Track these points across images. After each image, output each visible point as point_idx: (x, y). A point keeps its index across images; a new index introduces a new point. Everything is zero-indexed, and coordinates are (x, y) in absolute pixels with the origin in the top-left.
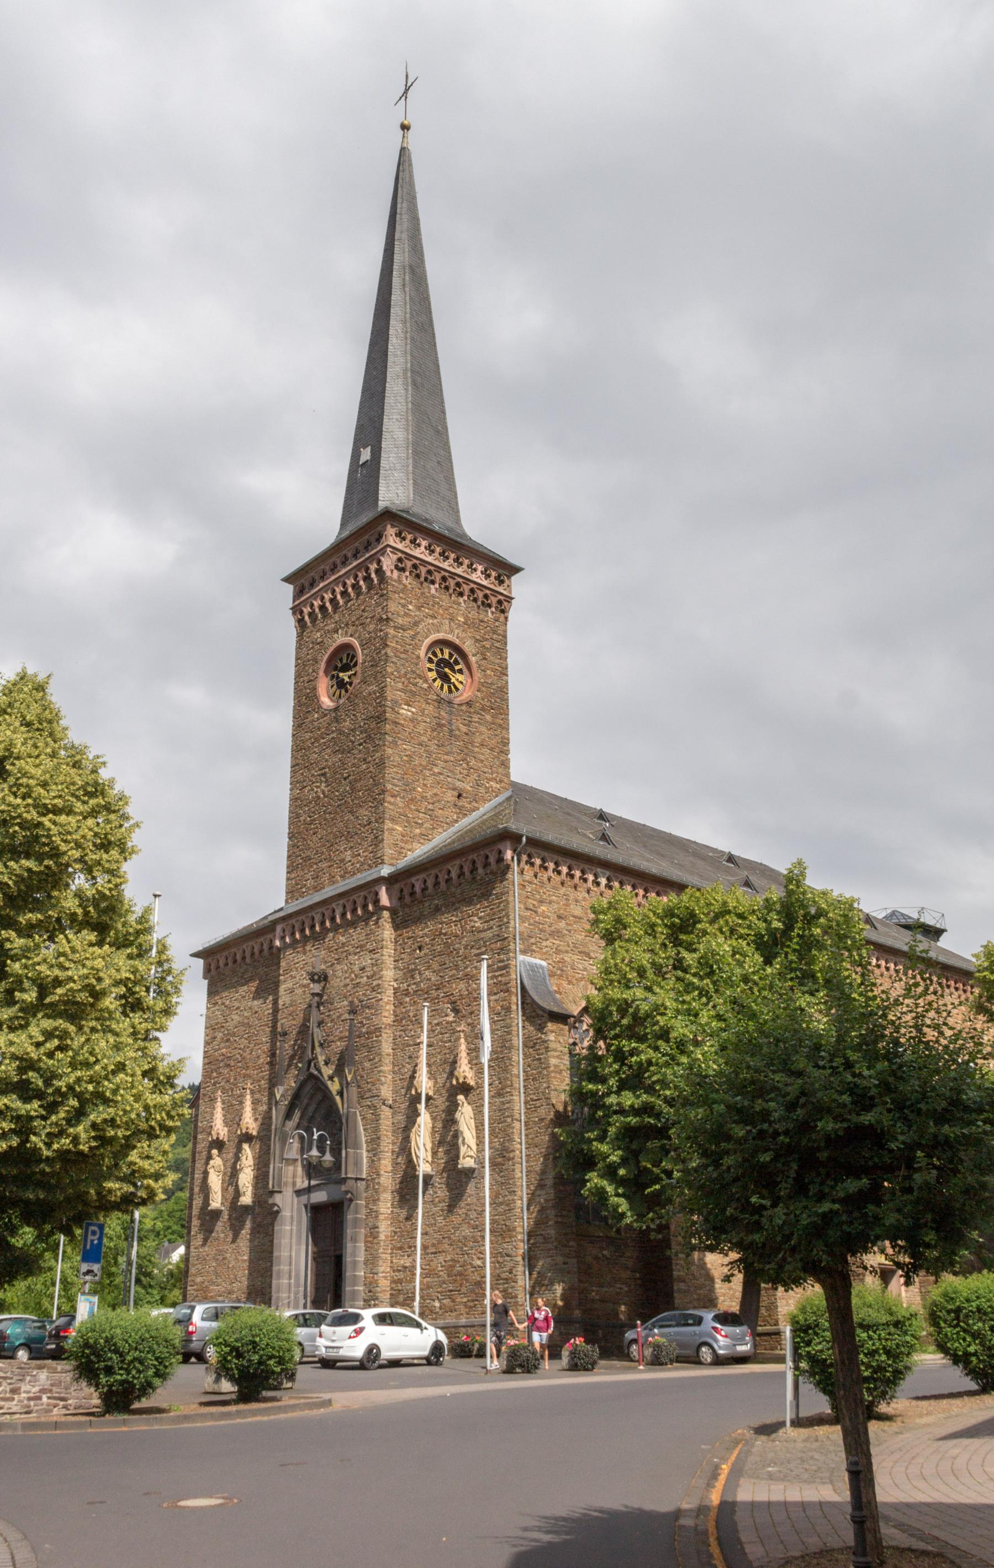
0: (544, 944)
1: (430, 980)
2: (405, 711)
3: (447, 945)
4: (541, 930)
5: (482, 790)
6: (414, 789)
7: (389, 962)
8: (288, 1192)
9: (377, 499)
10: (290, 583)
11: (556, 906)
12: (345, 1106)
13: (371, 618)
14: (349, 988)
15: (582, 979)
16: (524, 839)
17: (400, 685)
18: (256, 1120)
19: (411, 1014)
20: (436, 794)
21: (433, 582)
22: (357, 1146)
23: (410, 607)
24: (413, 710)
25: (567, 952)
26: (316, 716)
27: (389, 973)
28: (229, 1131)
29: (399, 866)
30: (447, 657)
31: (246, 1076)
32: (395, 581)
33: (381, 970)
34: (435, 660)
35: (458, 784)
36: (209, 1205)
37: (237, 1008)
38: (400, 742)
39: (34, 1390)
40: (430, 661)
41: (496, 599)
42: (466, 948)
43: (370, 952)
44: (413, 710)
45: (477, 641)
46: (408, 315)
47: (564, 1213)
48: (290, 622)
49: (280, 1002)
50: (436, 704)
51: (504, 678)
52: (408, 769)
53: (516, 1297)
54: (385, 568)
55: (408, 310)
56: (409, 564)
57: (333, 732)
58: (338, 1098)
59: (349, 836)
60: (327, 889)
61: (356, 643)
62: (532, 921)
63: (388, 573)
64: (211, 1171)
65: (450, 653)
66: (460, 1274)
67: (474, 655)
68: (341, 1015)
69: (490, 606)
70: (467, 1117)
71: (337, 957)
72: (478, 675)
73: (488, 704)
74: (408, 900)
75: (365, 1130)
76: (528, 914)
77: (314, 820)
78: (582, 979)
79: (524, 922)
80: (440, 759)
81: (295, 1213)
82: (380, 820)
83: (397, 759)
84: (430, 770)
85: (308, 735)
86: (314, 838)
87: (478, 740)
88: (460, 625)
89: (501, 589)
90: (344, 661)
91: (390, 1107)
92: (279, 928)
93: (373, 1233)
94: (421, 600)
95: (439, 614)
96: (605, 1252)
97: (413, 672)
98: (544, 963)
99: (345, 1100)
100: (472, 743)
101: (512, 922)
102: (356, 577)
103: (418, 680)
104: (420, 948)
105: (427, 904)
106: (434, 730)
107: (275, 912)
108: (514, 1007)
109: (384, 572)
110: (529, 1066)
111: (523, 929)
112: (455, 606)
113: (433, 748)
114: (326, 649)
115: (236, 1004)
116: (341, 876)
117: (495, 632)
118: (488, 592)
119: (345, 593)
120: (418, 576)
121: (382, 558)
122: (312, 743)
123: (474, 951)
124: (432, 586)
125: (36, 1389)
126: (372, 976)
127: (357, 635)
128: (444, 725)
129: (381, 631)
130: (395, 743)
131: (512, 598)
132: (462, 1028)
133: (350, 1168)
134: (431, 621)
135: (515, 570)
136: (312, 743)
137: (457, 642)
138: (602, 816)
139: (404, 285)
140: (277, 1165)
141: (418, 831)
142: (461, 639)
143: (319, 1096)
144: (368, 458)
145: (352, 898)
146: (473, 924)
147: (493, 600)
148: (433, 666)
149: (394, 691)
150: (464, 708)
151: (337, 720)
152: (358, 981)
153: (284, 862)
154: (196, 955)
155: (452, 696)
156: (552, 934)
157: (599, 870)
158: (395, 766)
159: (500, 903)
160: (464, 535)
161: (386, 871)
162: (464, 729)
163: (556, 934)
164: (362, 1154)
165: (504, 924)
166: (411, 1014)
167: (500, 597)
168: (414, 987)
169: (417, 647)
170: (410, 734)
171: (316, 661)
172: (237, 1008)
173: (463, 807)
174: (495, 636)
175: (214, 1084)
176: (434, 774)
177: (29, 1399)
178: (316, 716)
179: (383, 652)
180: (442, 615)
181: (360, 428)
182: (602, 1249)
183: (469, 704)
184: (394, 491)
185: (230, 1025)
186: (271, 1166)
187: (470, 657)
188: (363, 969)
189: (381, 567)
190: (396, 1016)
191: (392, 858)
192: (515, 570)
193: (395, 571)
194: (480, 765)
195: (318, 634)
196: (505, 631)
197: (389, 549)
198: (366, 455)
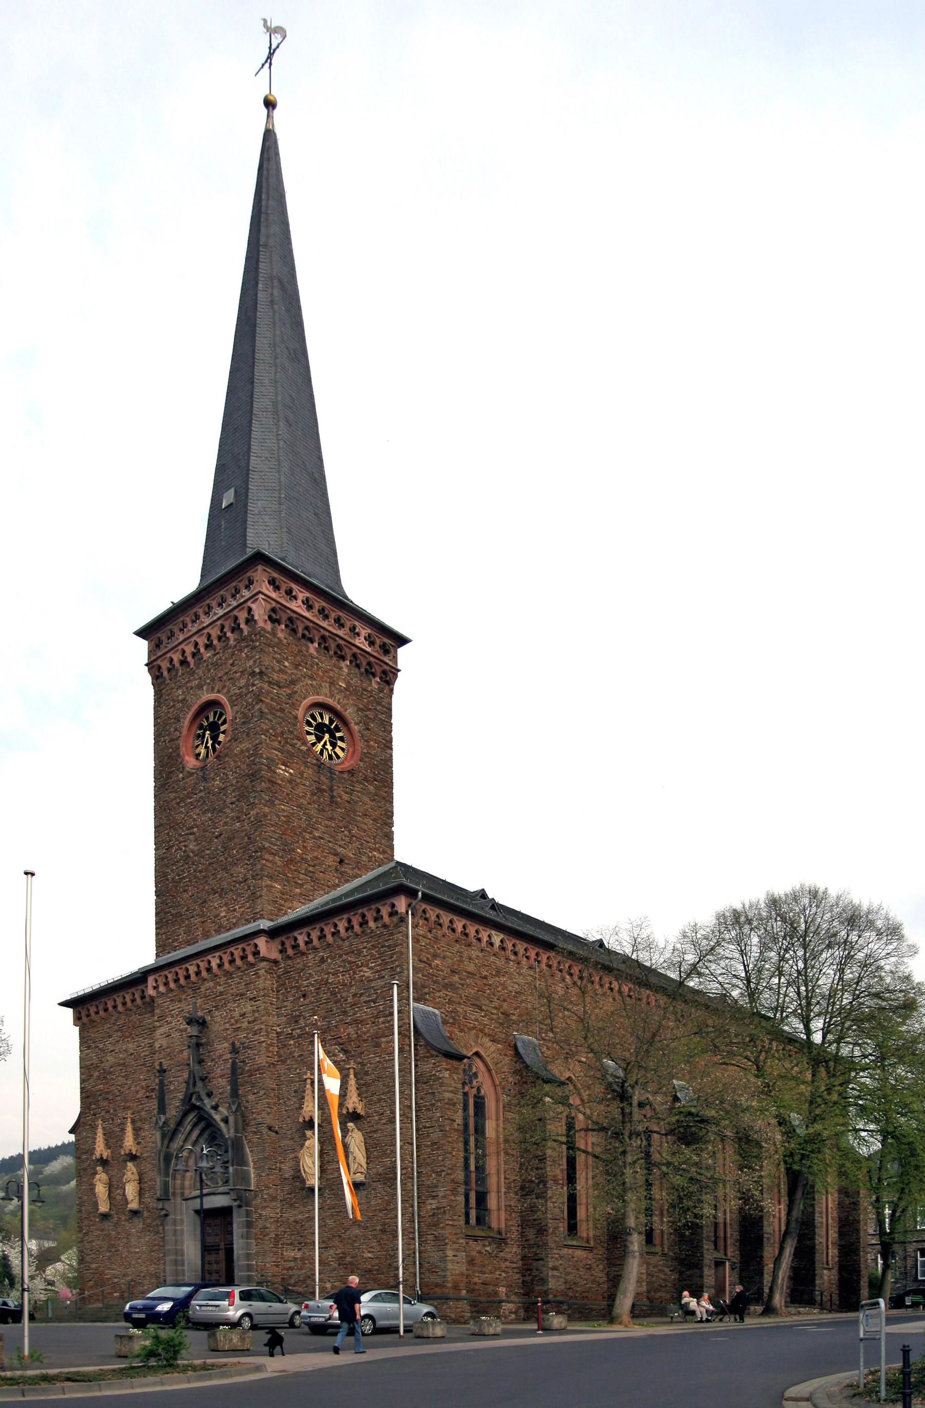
0: (437, 994)
3: (334, 994)
4: (435, 982)
6: (294, 850)
9: (245, 545)
10: (144, 638)
11: (450, 961)
14: (229, 1032)
15: (473, 1028)
17: (276, 744)
19: (296, 1055)
20: (316, 858)
21: (311, 641)
23: (286, 664)
24: (292, 771)
25: (459, 1003)
26: (181, 775)
30: (327, 722)
31: (126, 1108)
35: (339, 850)
36: (98, 1209)
37: (111, 1051)
38: (277, 802)
40: (309, 724)
41: (381, 669)
43: (251, 999)
44: (292, 771)
45: (359, 709)
46: (277, 339)
47: (455, 1218)
48: (146, 679)
50: (316, 768)
51: (388, 751)
52: (286, 830)
54: (256, 617)
56: (284, 617)
57: (201, 791)
59: (222, 893)
60: (200, 943)
61: (223, 698)
63: (261, 624)
66: (351, 1263)
67: (356, 724)
68: (221, 1056)
69: (374, 675)
70: (357, 1141)
71: (214, 1004)
72: (360, 745)
73: (372, 775)
74: (290, 952)
75: (251, 1151)
77: (184, 878)
78: (473, 1028)
79: (417, 973)
80: (320, 823)
83: (275, 818)
84: (310, 833)
85: (172, 795)
86: (185, 895)
87: (360, 809)
88: (341, 691)
89: (386, 659)
90: (211, 719)
91: (276, 1132)
92: (151, 980)
94: (298, 658)
95: (318, 675)
96: (488, 1249)
97: (292, 732)
98: (437, 1011)
100: (354, 811)
102: (223, 627)
103: (296, 741)
104: (304, 996)
105: (310, 957)
106: (313, 794)
109: (255, 622)
112: (336, 670)
114: (189, 707)
115: (111, 1048)
117: (379, 704)
118: (372, 659)
120: (294, 631)
121: (253, 606)
123: (364, 998)
124: (310, 645)
126: (254, 1021)
127: (225, 690)
128: (324, 791)
129: (253, 685)
131: (399, 671)
135: (403, 641)
136: (178, 804)
137: (339, 707)
142: (344, 706)
143: (202, 1124)
144: (231, 501)
145: (228, 951)
146: (362, 974)
148: (311, 730)
150: (345, 776)
151: (205, 779)
154: (65, 1004)
156: (446, 986)
157: (493, 932)
158: (272, 825)
159: (393, 954)
160: (346, 597)
162: (346, 797)
163: (450, 986)
164: (248, 1172)
166: (296, 1055)
167: (385, 667)
168: (298, 1031)
169: (295, 706)
170: (288, 794)
171: (178, 719)
172: (111, 1051)
173: (345, 872)
174: (379, 708)
175: (94, 1115)
176: (314, 837)
178: (181, 775)
180: (322, 678)
182: (484, 1246)
183: (351, 772)
184: (261, 537)
185: (106, 1065)
187: (352, 725)
188: (243, 1015)
189: (253, 616)
191: (272, 914)
192: (403, 641)
193: (269, 622)
195: (180, 692)
196: (390, 704)
197: (261, 596)
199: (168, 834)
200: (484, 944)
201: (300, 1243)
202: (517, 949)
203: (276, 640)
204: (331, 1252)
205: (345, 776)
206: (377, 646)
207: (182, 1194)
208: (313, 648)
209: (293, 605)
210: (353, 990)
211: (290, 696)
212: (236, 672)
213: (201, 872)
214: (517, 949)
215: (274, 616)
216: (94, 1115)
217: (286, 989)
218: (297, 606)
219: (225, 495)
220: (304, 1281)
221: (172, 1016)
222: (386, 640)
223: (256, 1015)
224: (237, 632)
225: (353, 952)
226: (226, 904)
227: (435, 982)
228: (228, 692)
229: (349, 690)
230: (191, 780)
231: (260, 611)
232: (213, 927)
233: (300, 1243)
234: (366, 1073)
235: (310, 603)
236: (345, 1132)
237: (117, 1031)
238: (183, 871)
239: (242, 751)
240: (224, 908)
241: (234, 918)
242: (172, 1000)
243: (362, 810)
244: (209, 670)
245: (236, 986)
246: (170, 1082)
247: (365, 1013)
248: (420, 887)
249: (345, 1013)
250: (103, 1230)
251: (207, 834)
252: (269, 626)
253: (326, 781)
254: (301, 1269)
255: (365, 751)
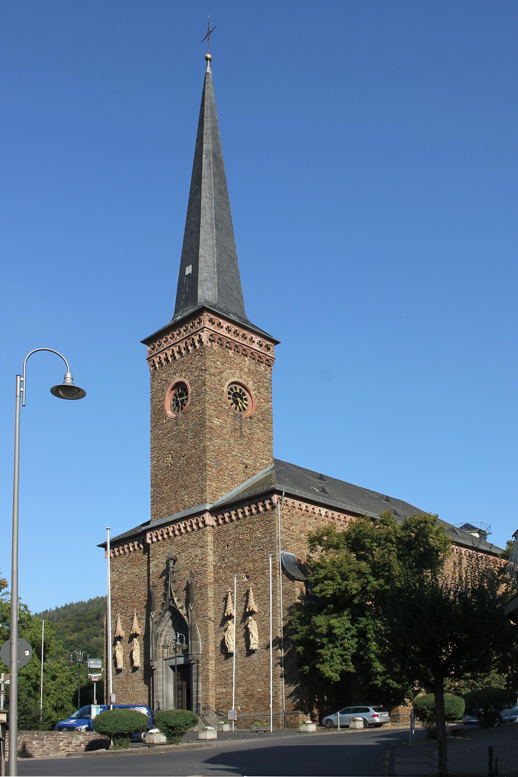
1: (233, 561)
2: (216, 422)
5: (258, 464)
7: (211, 552)
8: (160, 660)
11: (300, 526)
12: (190, 621)
13: (196, 368)
16: (284, 493)
17: (213, 407)
18: (140, 627)
19: (223, 578)
20: (233, 466)
22: (196, 639)
23: (218, 363)
24: (221, 421)
27: (211, 558)
28: (125, 632)
29: (215, 504)
32: (209, 348)
33: (207, 556)
34: (232, 393)
35: (245, 461)
37: (126, 573)
39: (78, 742)
42: (252, 546)
44: (221, 421)
48: (147, 368)
49: (151, 571)
53: (279, 704)
54: (203, 340)
55: (213, 181)
56: (217, 338)
57: (175, 431)
58: (185, 617)
59: (186, 487)
61: (187, 382)
62: (287, 534)
63: (205, 343)
64: (118, 651)
65: (240, 389)
66: (251, 695)
75: (200, 632)
76: (285, 530)
81: (164, 670)
82: (204, 480)
83: (213, 448)
86: (166, 487)
87: (256, 437)
91: (213, 621)
92: (148, 535)
93: (206, 678)
99: (190, 618)
100: (253, 439)
101: (277, 535)
103: (223, 404)
107: (143, 525)
108: (278, 575)
110: (285, 603)
111: (282, 538)
112: (243, 363)
113: (232, 442)
115: (125, 571)
116: (183, 508)
119: (180, 352)
121: (201, 334)
122: (163, 437)
123: (257, 548)
124: (230, 351)
125: (79, 742)
126: (202, 559)
127: (187, 377)
129: (202, 376)
130: (211, 439)
132: (251, 585)
133: (193, 649)
134: (229, 371)
136: (163, 437)
137: (244, 383)
138: (321, 477)
139: (210, 164)
140: (154, 648)
141: (224, 486)
147: (264, 359)
149: (210, 409)
152: (194, 561)
153: (149, 500)
155: (241, 413)
156: (297, 540)
157: (321, 508)
161: (208, 507)
162: (248, 431)
165: (272, 534)
166: (223, 578)
170: (219, 434)
171: (163, 390)
172: (126, 573)
174: (265, 380)
175: (115, 610)
177: (76, 746)
179: (203, 388)
180: (236, 368)
181: (184, 253)
186: (151, 649)
189: (201, 339)
190: (215, 579)
191: (211, 500)
193: (209, 342)
194: (257, 451)
195: (164, 375)
197: (205, 329)
198: (189, 270)
199: (158, 453)
200: (317, 515)
201: (225, 684)
202: (334, 516)
203: (213, 351)
204: (241, 689)
205: (248, 420)
206: (263, 347)
207: (163, 657)
208: (231, 352)
209: (221, 331)
210: (252, 543)
211: (220, 380)
212: (192, 368)
213: (175, 475)
214: (334, 516)
215: (211, 338)
216: (115, 610)
217: (218, 542)
218: (223, 332)
219: (187, 268)
220: (226, 706)
221: (159, 555)
222: (268, 343)
223: (203, 556)
224: (193, 347)
225: (251, 523)
226: (188, 494)
227: (291, 538)
228: (189, 378)
229: (250, 373)
230: (170, 425)
231: (205, 336)
232: (181, 506)
233: (225, 684)
234: (258, 589)
235: (230, 329)
236: (114, 644)
237: (129, 562)
238: (165, 474)
239: (196, 411)
240: (187, 496)
241: (192, 501)
242: (159, 546)
243: (257, 438)
244: (179, 365)
245: (193, 539)
246: (158, 592)
247: (257, 556)
248: (284, 490)
249: (248, 555)
250: (119, 678)
251: (178, 455)
252: (209, 344)
253: (238, 424)
254: (225, 699)
255: (258, 405)
